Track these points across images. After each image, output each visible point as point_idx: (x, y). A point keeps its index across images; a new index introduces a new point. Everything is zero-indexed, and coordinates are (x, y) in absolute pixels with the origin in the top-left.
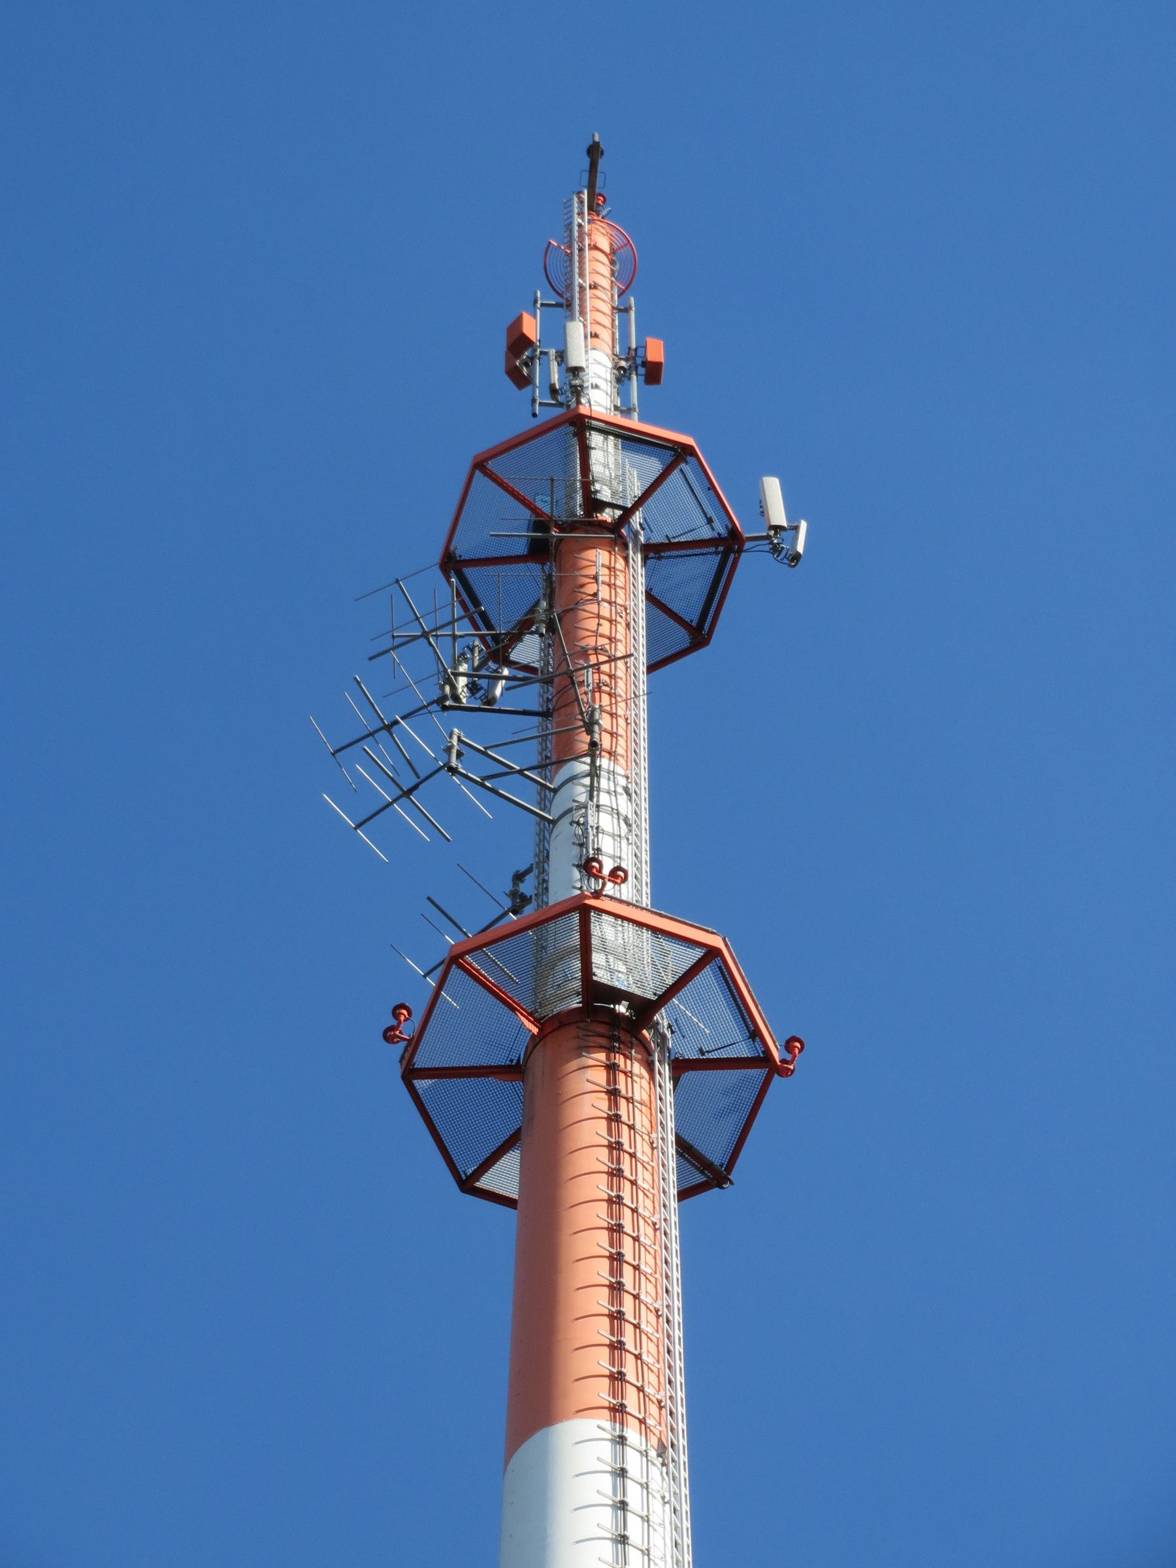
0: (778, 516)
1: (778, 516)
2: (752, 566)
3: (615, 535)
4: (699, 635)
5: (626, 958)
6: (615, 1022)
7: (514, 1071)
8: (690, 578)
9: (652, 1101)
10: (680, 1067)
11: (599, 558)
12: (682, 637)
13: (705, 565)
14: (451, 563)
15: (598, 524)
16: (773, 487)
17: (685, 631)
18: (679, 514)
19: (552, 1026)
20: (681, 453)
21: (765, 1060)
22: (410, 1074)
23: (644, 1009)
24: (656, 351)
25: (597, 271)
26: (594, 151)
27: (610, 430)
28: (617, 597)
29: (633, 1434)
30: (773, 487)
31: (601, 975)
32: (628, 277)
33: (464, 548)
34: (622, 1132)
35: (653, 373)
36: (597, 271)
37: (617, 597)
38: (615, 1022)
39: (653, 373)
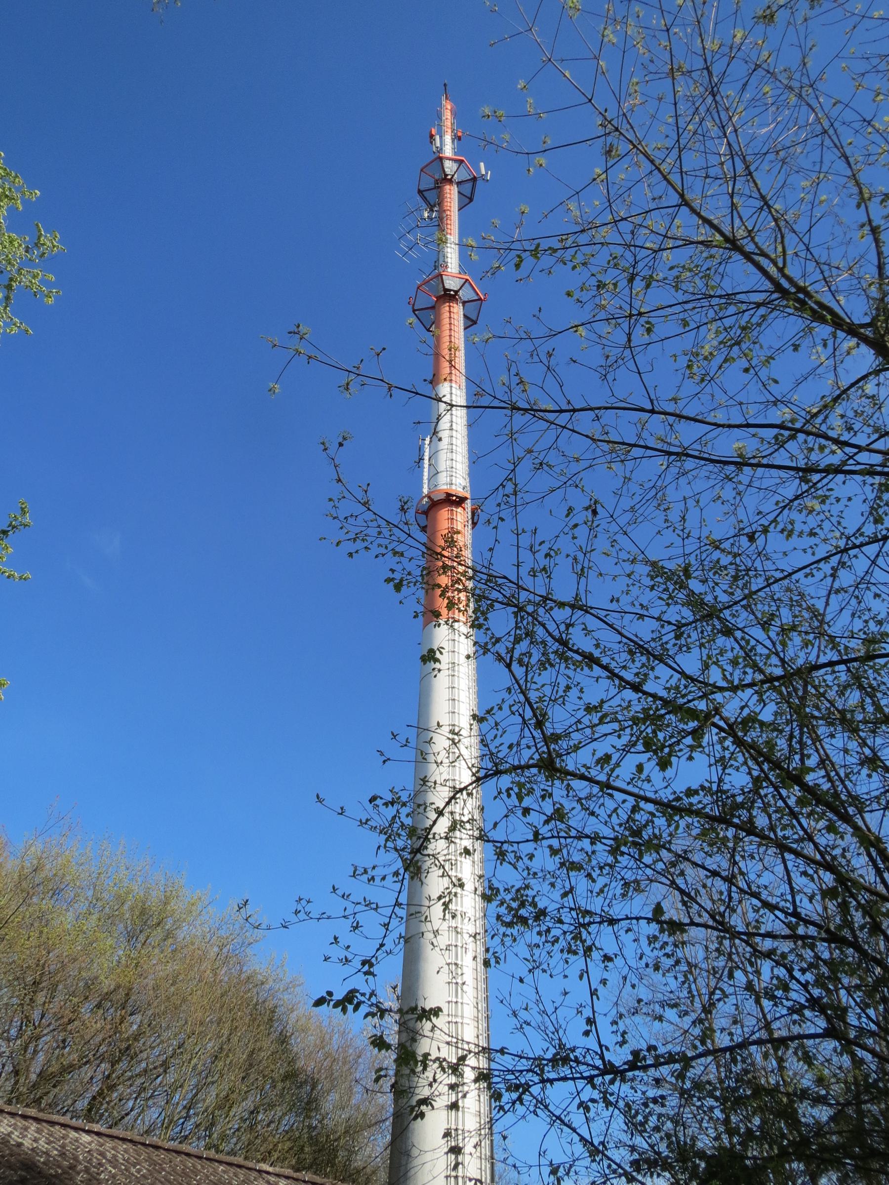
0: (483, 172)
1: (483, 172)
2: (479, 183)
3: (450, 181)
4: (471, 199)
5: (451, 284)
6: (449, 296)
7: (433, 308)
8: (467, 188)
9: (458, 310)
10: (464, 303)
11: (448, 187)
12: (467, 200)
13: (470, 185)
14: (420, 192)
15: (446, 180)
16: (482, 164)
17: (467, 200)
18: (463, 175)
19: (439, 298)
20: (462, 161)
21: (480, 299)
22: (414, 311)
23: (456, 292)
24: (460, 134)
25: (447, 116)
26: (445, 85)
27: (450, 159)
28: (452, 194)
29: (454, 385)
30: (482, 164)
31: (447, 286)
32: (454, 114)
33: (422, 188)
34: (454, 317)
35: (459, 138)
36: (447, 116)
37: (452, 194)
38: (449, 296)
39: (459, 138)
